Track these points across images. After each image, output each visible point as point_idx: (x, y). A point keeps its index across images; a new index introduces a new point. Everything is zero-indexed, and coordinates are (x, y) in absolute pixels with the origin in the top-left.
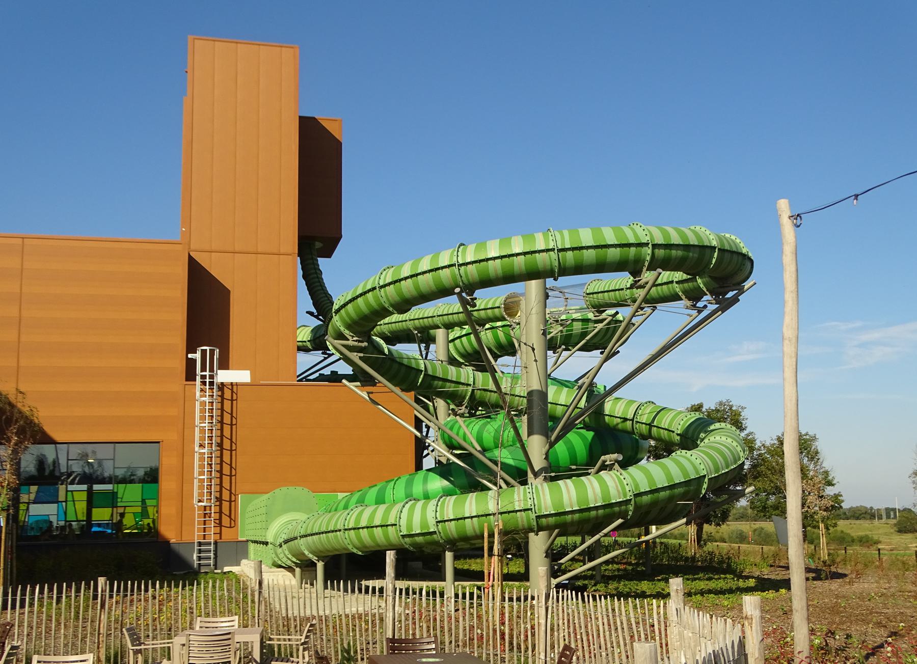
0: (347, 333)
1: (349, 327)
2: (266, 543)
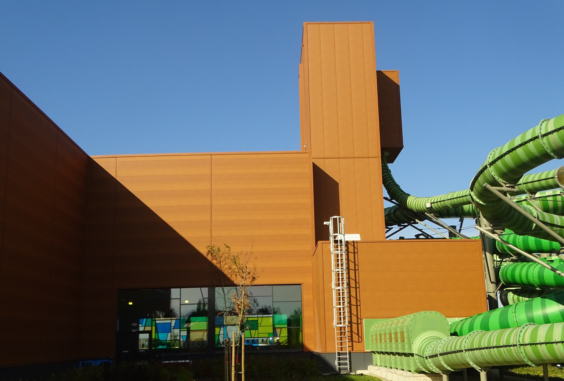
0: (500, 180)
1: (503, 175)
2: (412, 355)
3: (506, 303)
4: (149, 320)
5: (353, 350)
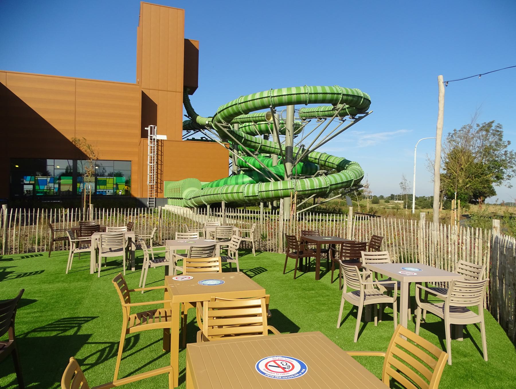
0: (222, 121)
1: (224, 119)
4: (33, 177)
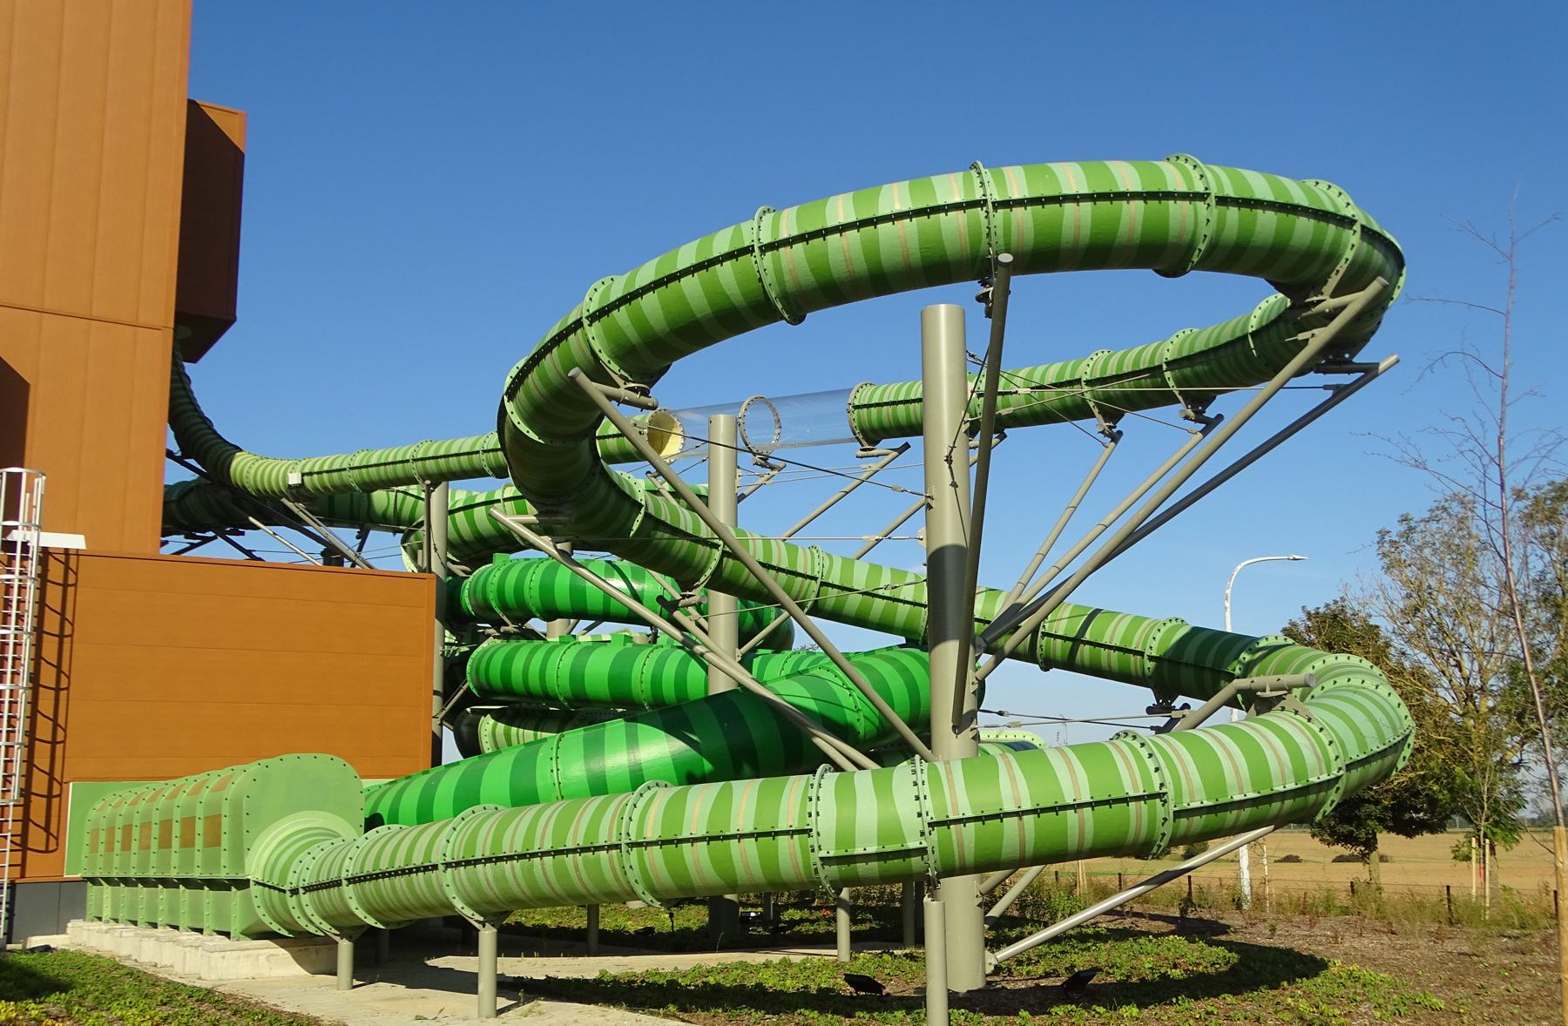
0: (613, 368)
2: (243, 884)
3: (469, 746)
5: (23, 876)
